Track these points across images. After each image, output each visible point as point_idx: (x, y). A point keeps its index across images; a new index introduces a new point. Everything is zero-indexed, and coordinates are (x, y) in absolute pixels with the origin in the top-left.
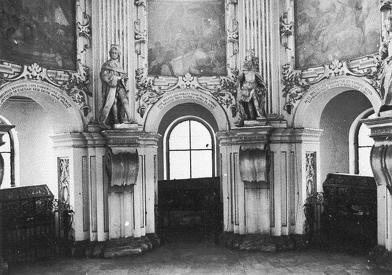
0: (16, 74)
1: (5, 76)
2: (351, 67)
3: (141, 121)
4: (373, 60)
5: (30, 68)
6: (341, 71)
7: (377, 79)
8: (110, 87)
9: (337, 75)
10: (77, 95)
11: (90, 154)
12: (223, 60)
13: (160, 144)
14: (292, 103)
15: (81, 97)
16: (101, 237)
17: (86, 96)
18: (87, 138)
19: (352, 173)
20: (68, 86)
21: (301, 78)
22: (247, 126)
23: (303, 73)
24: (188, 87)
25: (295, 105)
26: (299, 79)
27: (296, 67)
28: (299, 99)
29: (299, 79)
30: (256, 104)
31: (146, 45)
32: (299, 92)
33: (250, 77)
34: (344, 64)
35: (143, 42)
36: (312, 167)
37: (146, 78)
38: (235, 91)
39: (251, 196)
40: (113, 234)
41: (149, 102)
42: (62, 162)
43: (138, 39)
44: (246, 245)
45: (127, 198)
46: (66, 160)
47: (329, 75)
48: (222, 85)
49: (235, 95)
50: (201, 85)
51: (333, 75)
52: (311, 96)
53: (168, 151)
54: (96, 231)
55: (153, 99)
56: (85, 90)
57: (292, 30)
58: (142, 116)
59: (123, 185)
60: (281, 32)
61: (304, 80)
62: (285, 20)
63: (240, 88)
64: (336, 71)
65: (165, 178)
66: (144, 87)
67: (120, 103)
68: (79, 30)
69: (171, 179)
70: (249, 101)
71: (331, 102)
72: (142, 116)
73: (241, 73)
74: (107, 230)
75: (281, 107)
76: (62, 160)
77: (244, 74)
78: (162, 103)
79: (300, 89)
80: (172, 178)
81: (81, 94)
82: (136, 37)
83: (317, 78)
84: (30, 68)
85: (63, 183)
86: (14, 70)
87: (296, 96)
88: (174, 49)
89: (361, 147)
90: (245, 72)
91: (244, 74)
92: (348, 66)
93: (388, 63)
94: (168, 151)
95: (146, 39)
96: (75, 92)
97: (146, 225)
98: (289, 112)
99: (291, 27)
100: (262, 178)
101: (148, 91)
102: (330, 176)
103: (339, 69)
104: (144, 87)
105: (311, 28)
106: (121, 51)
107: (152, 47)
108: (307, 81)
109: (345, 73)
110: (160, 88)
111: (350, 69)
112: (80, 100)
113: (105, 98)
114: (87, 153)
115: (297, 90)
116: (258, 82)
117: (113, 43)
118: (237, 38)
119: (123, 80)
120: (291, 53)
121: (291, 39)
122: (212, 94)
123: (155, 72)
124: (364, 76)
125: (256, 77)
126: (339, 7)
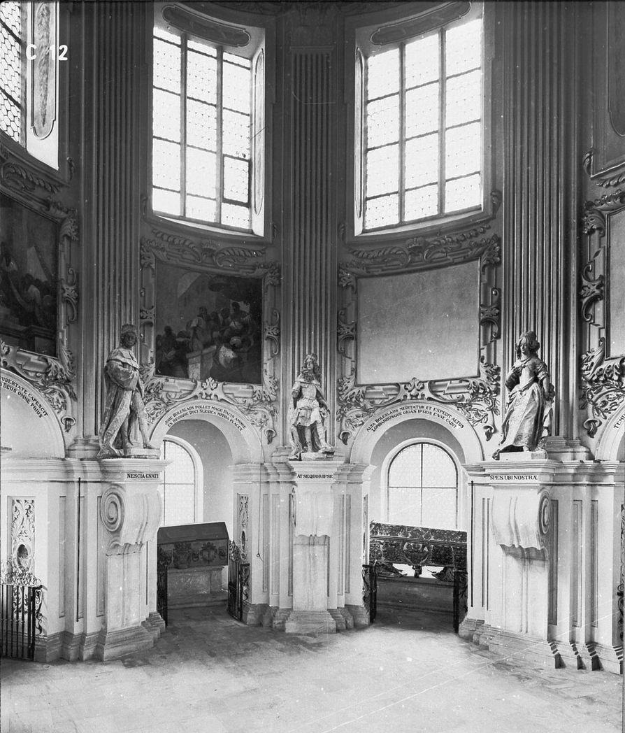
4: (467, 383)
5: (204, 384)
6: (420, 393)
7: (470, 409)
10: (55, 396)
15: (61, 400)
25: (354, 433)
26: (361, 400)
29: (361, 400)
32: (359, 417)
42: (17, 504)
48: (255, 399)
51: (409, 397)
55: (159, 410)
61: (366, 401)
64: (413, 393)
70: (308, 425)
75: (336, 434)
76: (18, 501)
79: (360, 413)
85: (17, 539)
88: (190, 340)
90: (303, 385)
91: (301, 388)
96: (54, 391)
98: (345, 441)
101: (153, 399)
105: (430, 354)
108: (372, 403)
109: (426, 397)
111: (432, 392)
112: (60, 406)
117: (128, 322)
124: (452, 403)
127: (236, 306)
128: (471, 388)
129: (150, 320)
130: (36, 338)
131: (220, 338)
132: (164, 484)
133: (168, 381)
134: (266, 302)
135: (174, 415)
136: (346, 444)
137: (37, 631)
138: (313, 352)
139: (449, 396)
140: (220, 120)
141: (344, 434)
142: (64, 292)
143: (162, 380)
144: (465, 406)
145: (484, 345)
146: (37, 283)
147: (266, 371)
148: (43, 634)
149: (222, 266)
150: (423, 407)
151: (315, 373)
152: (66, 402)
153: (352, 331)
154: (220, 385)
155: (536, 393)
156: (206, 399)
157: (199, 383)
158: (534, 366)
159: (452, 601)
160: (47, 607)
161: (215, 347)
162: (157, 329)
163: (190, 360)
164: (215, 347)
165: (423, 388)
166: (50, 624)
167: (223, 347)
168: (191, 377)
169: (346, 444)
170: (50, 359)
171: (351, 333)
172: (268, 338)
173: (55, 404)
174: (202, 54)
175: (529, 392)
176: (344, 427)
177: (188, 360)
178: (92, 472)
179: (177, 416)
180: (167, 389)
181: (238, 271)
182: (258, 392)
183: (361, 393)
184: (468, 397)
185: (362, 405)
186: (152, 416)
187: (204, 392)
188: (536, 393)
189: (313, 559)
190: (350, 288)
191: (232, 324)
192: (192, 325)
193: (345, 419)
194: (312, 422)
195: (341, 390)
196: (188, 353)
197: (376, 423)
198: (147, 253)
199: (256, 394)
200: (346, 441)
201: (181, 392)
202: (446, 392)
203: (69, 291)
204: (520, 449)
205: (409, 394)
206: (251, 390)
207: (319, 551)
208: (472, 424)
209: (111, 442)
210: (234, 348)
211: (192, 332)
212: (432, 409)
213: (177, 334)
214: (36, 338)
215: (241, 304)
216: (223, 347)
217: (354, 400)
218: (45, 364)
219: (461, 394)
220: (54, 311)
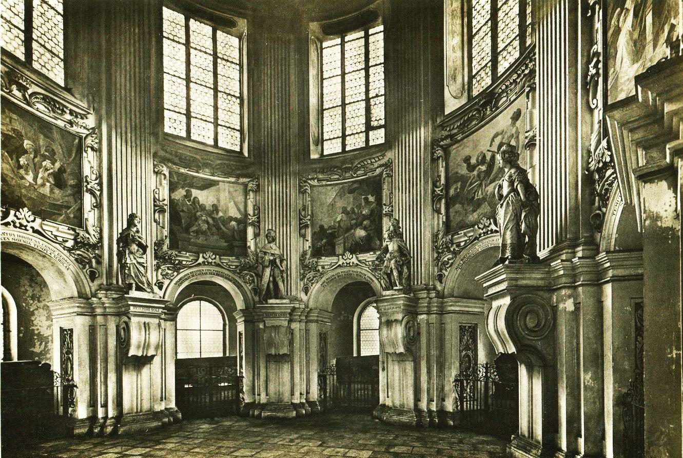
0: (193, 261)
1: (184, 263)
3: (304, 297)
5: (344, 257)
14: (444, 271)
17: (255, 278)
21: (452, 244)
22: (385, 296)
25: (446, 274)
27: (447, 232)
28: (450, 266)
30: (395, 273)
31: (310, 230)
37: (309, 260)
45: (286, 367)
52: (462, 262)
53: (359, 330)
54: (105, 406)
56: (254, 273)
58: (306, 295)
59: (142, 355)
65: (355, 355)
69: (362, 355)
77: (387, 245)
78: (324, 282)
79: (450, 256)
81: (251, 276)
82: (301, 222)
84: (205, 255)
86: (191, 258)
87: (447, 265)
94: (359, 330)
116: (403, 252)
117: (270, 228)
120: (443, 218)
125: (399, 247)
127: (366, 199)
132: (200, 330)
135: (327, 279)
140: (188, 55)
146: (235, 219)
152: (254, 279)
174: (201, 31)
180: (322, 264)
185: (452, 249)
187: (345, 262)
191: (364, 212)
193: (440, 263)
203: (252, 219)
210: (365, 228)
220: (245, 232)
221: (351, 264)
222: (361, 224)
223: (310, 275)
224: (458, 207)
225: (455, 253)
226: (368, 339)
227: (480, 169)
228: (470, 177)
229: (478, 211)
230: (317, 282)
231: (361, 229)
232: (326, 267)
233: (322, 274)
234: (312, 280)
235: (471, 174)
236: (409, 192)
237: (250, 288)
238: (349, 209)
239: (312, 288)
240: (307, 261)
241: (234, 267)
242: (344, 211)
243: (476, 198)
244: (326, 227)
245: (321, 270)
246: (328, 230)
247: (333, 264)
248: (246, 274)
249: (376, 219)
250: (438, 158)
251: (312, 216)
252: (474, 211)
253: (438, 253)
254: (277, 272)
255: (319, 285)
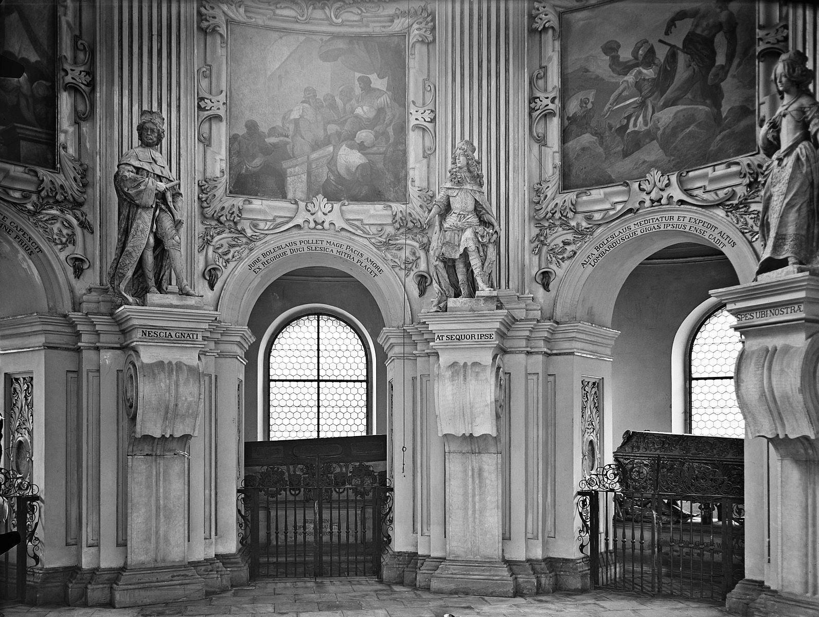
2: (689, 187)
6: (665, 194)
7: (746, 213)
8: (138, 206)
9: (656, 204)
10: (56, 227)
11: (86, 367)
12: (400, 161)
13: (251, 355)
15: (65, 232)
16: (109, 559)
18: (79, 328)
19: (677, 429)
20: (34, 205)
23: (579, 200)
24: (319, 227)
25: (560, 272)
28: (569, 258)
29: (570, 215)
30: (475, 262)
32: (569, 244)
33: (462, 202)
34: (674, 178)
35: (218, 118)
36: (595, 411)
37: (223, 201)
38: (425, 240)
39: (455, 466)
40: (139, 555)
41: (230, 256)
43: (204, 109)
44: (451, 270)
45: (176, 467)
46: (24, 379)
47: (637, 206)
49: (426, 247)
50: (351, 225)
51: (648, 203)
53: (268, 380)
55: (238, 248)
57: (555, 107)
58: (212, 287)
60: (532, 110)
61: (580, 216)
62: (541, 83)
63: (437, 228)
64: (653, 195)
66: (218, 220)
67: (160, 247)
68: (63, 74)
70: (457, 256)
71: (636, 274)
72: (212, 287)
73: (440, 197)
74: (122, 544)
76: (17, 380)
77: (448, 197)
79: (570, 237)
80: (275, 436)
83: (612, 213)
89: (697, 379)
90: (450, 192)
91: (448, 197)
92: (681, 182)
93: (779, 165)
94: (268, 380)
95: (222, 113)
97: (216, 534)
98: (546, 287)
99: (554, 98)
100: (485, 427)
101: (227, 231)
102: (630, 438)
103: (661, 190)
104: (218, 220)
106: (165, 127)
107: (241, 131)
108: (589, 219)
109: (675, 199)
110: (255, 226)
111: (686, 191)
112: (64, 240)
113: (125, 233)
114: (80, 362)
115: (563, 238)
118: (433, 120)
119: (169, 195)
121: (554, 127)
122: (373, 244)
123: (242, 185)
124: (718, 205)
126: (661, 53)
127: (366, 84)
128: (745, 176)
129: (219, 112)
130: (23, 143)
131: (339, 134)
132: (318, 381)
133: (250, 203)
134: (411, 71)
135: (264, 255)
136: (549, 291)
137: (31, 562)
138: (467, 138)
139: (712, 193)
141: (543, 273)
142: (67, 74)
143: (239, 201)
144: (736, 207)
145: (766, 95)
147: (413, 181)
148: (39, 566)
149: (340, 21)
150: (672, 218)
151: (470, 171)
152: (74, 234)
153: (553, 101)
154: (337, 206)
155: (803, 159)
156: (315, 228)
157: (302, 205)
158: (801, 110)
159: (140, 379)
160: (44, 528)
161: (331, 148)
162: (230, 126)
163: (289, 171)
164: (331, 148)
165: (668, 185)
166: (50, 555)
167: (344, 147)
168: (290, 195)
169: (549, 291)
170: (41, 171)
171: (551, 106)
172: (417, 127)
173: (55, 237)
175: (790, 161)
176: (543, 265)
177: (286, 170)
178: (106, 332)
179: (268, 258)
181: (367, 26)
182: (399, 215)
183: (568, 204)
184: (741, 191)
186: (226, 257)
187: (311, 218)
188: (803, 159)
189: (480, 475)
190: (550, 32)
191: (359, 111)
192: (292, 117)
193: (545, 249)
194: (462, 250)
195: (538, 203)
196: (285, 159)
197: (595, 252)
198: (211, 11)
199: (397, 218)
200: (548, 285)
201: (274, 220)
202: (708, 189)
204: (784, 263)
205: (647, 198)
206: (390, 212)
207: (490, 463)
208: (750, 238)
209: (122, 287)
211: (292, 127)
212: (687, 220)
213: (266, 131)
214: (23, 143)
215: (373, 77)
216: (344, 147)
217: (558, 215)
218: (35, 179)
219: (730, 189)
220: (52, 104)
221: (326, 225)
222: (352, 136)
223: (223, 239)
224: (587, 138)
225: (581, 233)
226: (304, 403)
227: (640, 73)
228: (617, 85)
229: (636, 155)
230: (241, 259)
231: (351, 147)
232: (262, 225)
233: (251, 240)
234: (226, 254)
235: (621, 79)
236: (480, 87)
237: (62, 256)
238: (320, 96)
239: (226, 272)
240: (216, 205)
241: (17, 195)
242: (310, 96)
243: (631, 128)
244: (264, 128)
245: (249, 233)
246: (270, 135)
247: (279, 220)
248: (54, 218)
249: (390, 131)
250: (545, 29)
251: (230, 96)
252: (626, 154)
253: (542, 228)
254: (167, 222)
255: (243, 266)
